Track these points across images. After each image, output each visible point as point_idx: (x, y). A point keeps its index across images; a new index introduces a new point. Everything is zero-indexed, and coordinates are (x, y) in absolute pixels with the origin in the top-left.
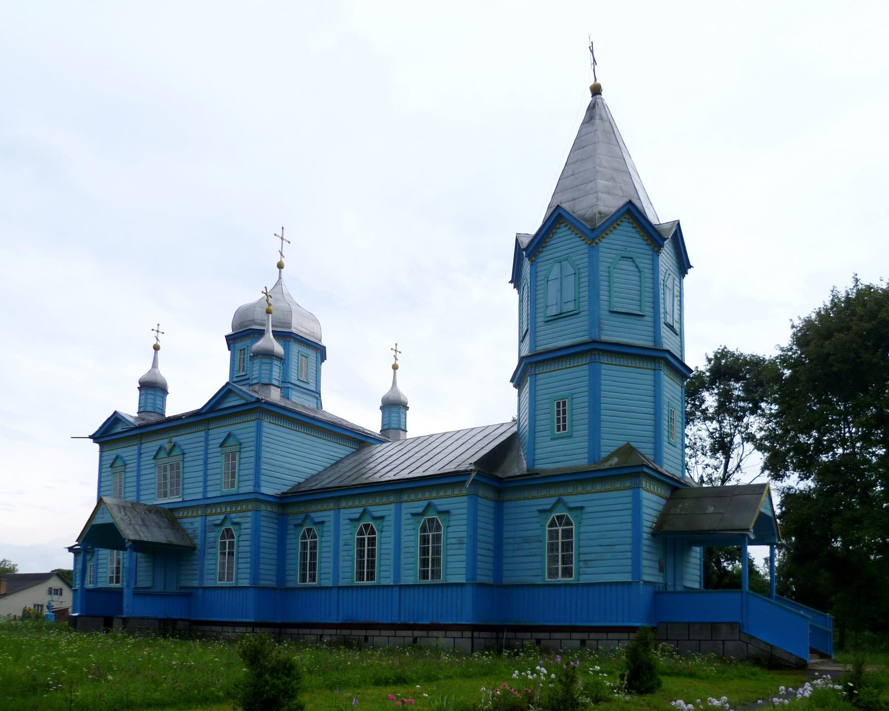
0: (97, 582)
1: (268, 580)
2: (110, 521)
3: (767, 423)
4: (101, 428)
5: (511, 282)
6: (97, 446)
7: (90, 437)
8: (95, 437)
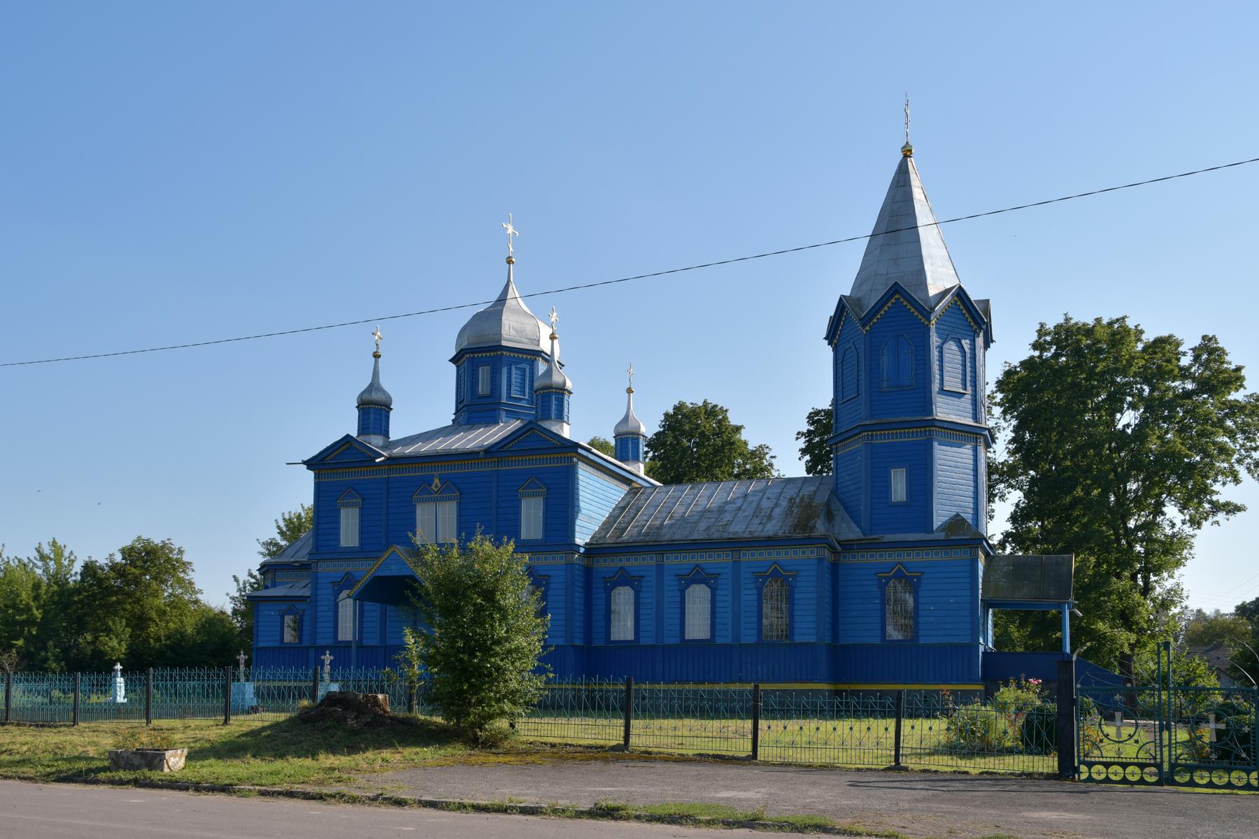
5: (826, 338)
6: (311, 474)
7: (304, 463)
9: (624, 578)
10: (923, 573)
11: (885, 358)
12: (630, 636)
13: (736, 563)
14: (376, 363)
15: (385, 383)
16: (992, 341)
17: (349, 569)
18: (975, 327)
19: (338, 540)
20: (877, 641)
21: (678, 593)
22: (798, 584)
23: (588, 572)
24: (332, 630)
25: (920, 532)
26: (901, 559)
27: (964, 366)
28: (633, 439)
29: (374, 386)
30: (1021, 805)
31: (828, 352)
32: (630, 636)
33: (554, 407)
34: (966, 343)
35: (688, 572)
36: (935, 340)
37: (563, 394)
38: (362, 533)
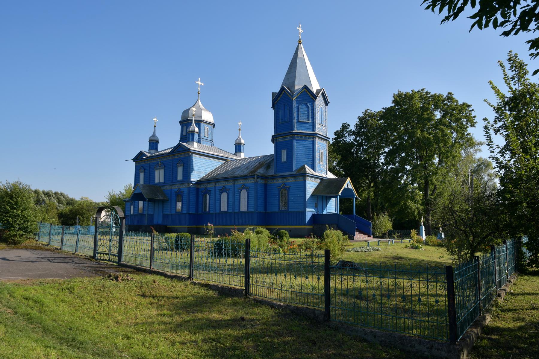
0: (182, 200)
1: (193, 212)
2: (140, 192)
3: (516, 72)
4: (136, 157)
5: (272, 107)
6: (134, 163)
7: (132, 160)
8: (134, 160)
9: (224, 190)
10: (290, 186)
11: (281, 112)
12: (226, 209)
13: (234, 185)
14: (155, 128)
15: (157, 134)
16: (329, 103)
17: (179, 187)
18: (313, 99)
19: (177, 178)
20: (277, 210)
21: (219, 196)
22: (250, 192)
23: (198, 189)
24: (238, 200)
25: (289, 172)
26: (284, 182)
27: (309, 112)
28: (239, 145)
29: (154, 135)
30: (62, 301)
31: (272, 112)
32: (226, 209)
33: (191, 138)
34: (309, 105)
35: (176, 191)
36: (295, 104)
37: (194, 133)
38: (183, 177)
